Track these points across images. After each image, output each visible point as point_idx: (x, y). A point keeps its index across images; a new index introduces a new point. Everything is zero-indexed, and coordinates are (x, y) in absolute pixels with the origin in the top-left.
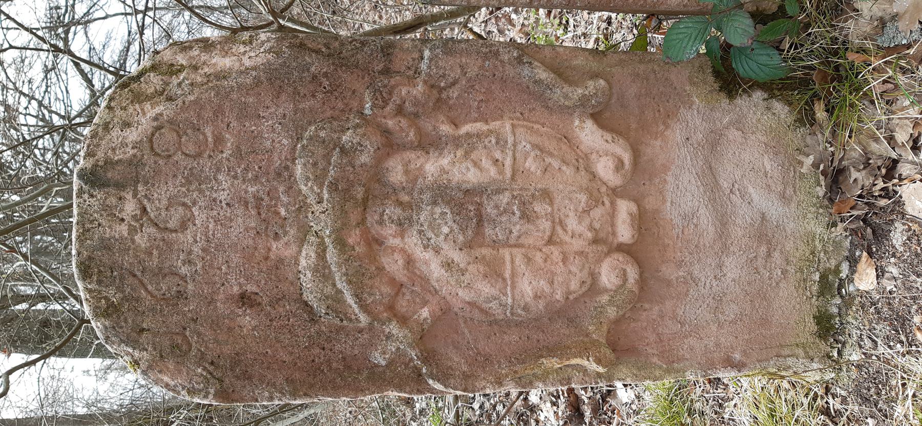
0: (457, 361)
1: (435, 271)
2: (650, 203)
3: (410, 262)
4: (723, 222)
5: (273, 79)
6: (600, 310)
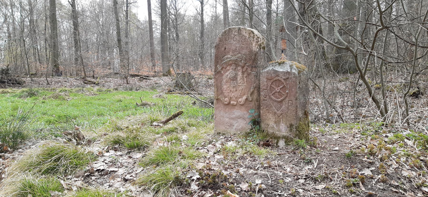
0: (217, 77)
1: (227, 73)
2: (236, 107)
3: (228, 70)
4: (233, 119)
5: (251, 51)
6: (222, 98)
